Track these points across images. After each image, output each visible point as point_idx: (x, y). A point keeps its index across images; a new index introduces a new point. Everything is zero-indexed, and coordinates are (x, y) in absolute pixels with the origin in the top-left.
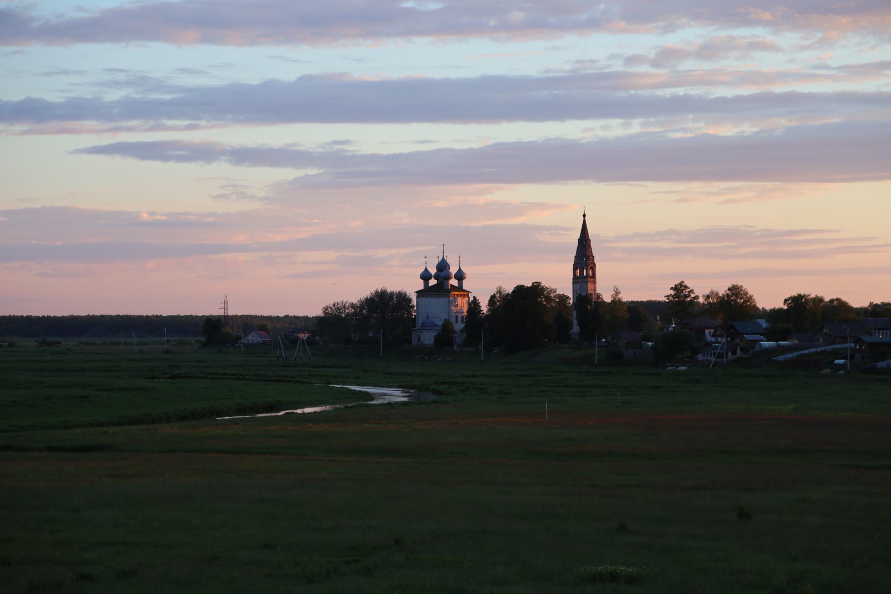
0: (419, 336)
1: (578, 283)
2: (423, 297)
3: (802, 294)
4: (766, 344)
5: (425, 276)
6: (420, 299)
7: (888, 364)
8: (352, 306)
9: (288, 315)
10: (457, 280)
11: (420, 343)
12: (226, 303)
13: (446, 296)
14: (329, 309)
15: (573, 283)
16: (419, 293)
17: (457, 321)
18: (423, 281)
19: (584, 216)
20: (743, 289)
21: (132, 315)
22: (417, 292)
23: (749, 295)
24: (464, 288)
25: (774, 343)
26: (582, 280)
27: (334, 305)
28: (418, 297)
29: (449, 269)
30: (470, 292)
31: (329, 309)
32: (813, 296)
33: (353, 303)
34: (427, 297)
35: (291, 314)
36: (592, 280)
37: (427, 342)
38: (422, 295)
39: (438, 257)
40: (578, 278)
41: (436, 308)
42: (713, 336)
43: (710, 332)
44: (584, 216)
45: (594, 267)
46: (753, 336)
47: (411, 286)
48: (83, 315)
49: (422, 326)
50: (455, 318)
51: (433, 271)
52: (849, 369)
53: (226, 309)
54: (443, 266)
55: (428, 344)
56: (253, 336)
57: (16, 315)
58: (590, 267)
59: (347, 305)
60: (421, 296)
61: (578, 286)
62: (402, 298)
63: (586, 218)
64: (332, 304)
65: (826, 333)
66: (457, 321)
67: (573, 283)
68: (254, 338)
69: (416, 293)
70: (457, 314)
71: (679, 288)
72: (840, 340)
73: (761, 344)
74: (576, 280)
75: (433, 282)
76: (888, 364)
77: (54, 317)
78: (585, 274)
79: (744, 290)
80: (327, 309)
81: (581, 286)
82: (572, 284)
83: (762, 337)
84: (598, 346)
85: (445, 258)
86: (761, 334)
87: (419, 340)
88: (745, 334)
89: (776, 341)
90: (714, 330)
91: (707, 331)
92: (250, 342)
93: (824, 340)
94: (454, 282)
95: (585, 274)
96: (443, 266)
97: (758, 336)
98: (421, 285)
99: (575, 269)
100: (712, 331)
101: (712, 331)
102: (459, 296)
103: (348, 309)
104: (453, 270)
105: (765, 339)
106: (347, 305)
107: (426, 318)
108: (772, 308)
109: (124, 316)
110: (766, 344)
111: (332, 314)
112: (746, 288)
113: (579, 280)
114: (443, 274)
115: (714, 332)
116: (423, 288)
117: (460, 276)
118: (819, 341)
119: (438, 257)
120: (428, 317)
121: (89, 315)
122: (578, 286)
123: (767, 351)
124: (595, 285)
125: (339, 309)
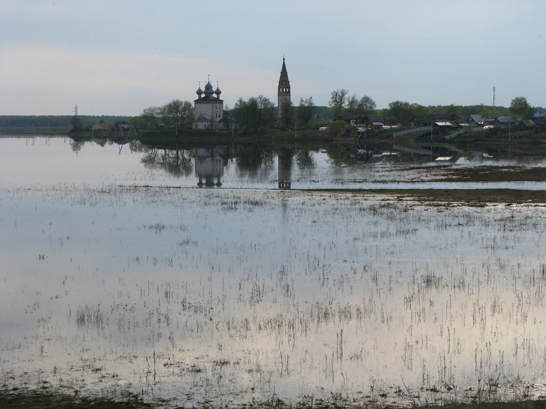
0: (197, 125)
2: (198, 103)
5: (199, 92)
6: (196, 104)
7: (451, 137)
9: (104, 116)
10: (216, 95)
12: (76, 108)
14: (147, 110)
16: (196, 102)
18: (198, 95)
19: (284, 59)
20: (370, 99)
21: (436, 105)
23: (373, 101)
24: (220, 99)
26: (283, 94)
27: (150, 108)
31: (147, 110)
32: (404, 102)
34: (200, 103)
35: (105, 115)
37: (201, 128)
39: (206, 82)
40: (281, 93)
41: (206, 110)
44: (284, 59)
47: (191, 97)
49: (198, 119)
51: (203, 89)
52: (509, 146)
53: (76, 111)
55: (201, 129)
56: (98, 126)
59: (157, 108)
60: (197, 103)
61: (281, 97)
62: (188, 105)
64: (148, 108)
65: (415, 122)
68: (97, 127)
69: (194, 102)
72: (422, 125)
75: (203, 95)
76: (451, 137)
77: (117, 116)
78: (284, 91)
79: (371, 99)
80: (146, 110)
81: (282, 98)
84: (508, 137)
87: (197, 127)
89: (390, 126)
90: (355, 120)
91: (351, 121)
92: (96, 129)
93: (415, 125)
94: (215, 95)
95: (284, 91)
97: (380, 123)
98: (197, 97)
99: (279, 88)
100: (354, 121)
101: (354, 121)
104: (214, 89)
105: (383, 125)
106: (157, 108)
107: (200, 115)
108: (465, 106)
109: (66, 116)
111: (148, 113)
112: (372, 98)
113: (281, 94)
114: (209, 91)
115: (355, 121)
116: (198, 99)
117: (218, 92)
118: (412, 125)
119: (206, 82)
120: (201, 115)
121: (114, 116)
122: (281, 97)
123: (385, 131)
125: (523, 98)
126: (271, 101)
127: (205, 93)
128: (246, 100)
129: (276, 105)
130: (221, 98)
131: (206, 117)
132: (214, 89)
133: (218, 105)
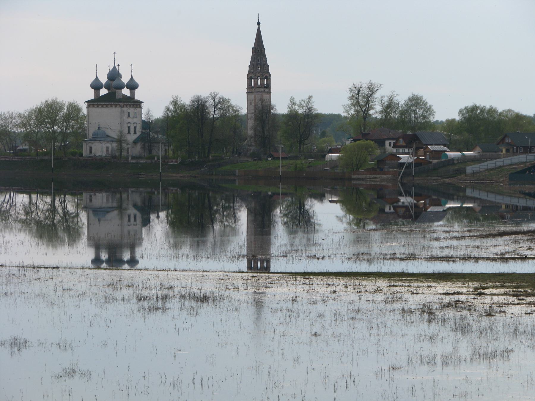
1: (252, 92)
2: (93, 107)
3: (478, 105)
4: (452, 154)
5: (96, 86)
6: (90, 109)
8: (20, 116)
11: (92, 155)
13: (118, 106)
15: (248, 93)
16: (91, 103)
17: (129, 132)
19: (259, 24)
22: (87, 102)
25: (460, 153)
26: (256, 90)
28: (88, 107)
29: (121, 78)
30: (143, 102)
33: (20, 114)
34: (98, 107)
36: (266, 90)
37: (98, 154)
38: (93, 105)
40: (252, 88)
42: (394, 147)
43: (390, 143)
44: (259, 24)
45: (268, 76)
46: (436, 146)
48: (327, 113)
49: (93, 137)
50: (127, 128)
51: (104, 80)
54: (114, 75)
57: (331, 113)
58: (264, 76)
60: (92, 106)
61: (252, 96)
62: (74, 109)
63: (261, 26)
66: (129, 132)
67: (248, 93)
69: (86, 103)
70: (129, 125)
71: (175, 103)
73: (446, 154)
74: (250, 89)
75: (104, 92)
79: (424, 101)
81: (255, 97)
82: (246, 94)
83: (445, 147)
85: (117, 67)
86: (444, 145)
87: (91, 152)
88: (429, 145)
90: (395, 141)
91: (387, 142)
93: (507, 151)
94: (126, 92)
96: (114, 75)
97: (442, 146)
98: (91, 95)
99: (249, 79)
101: (392, 142)
102: (131, 106)
103: (15, 119)
104: (125, 79)
105: (448, 150)
110: (452, 154)
113: (254, 90)
114: (114, 83)
116: (93, 98)
117: (133, 86)
118: (502, 152)
119: (109, 66)
120: (99, 128)
123: (451, 162)
124: (270, 95)
126: (233, 102)
127: (107, 87)
128: (186, 100)
129: (244, 111)
130: (137, 97)
131: (109, 132)
132: (125, 79)
133: (132, 110)
